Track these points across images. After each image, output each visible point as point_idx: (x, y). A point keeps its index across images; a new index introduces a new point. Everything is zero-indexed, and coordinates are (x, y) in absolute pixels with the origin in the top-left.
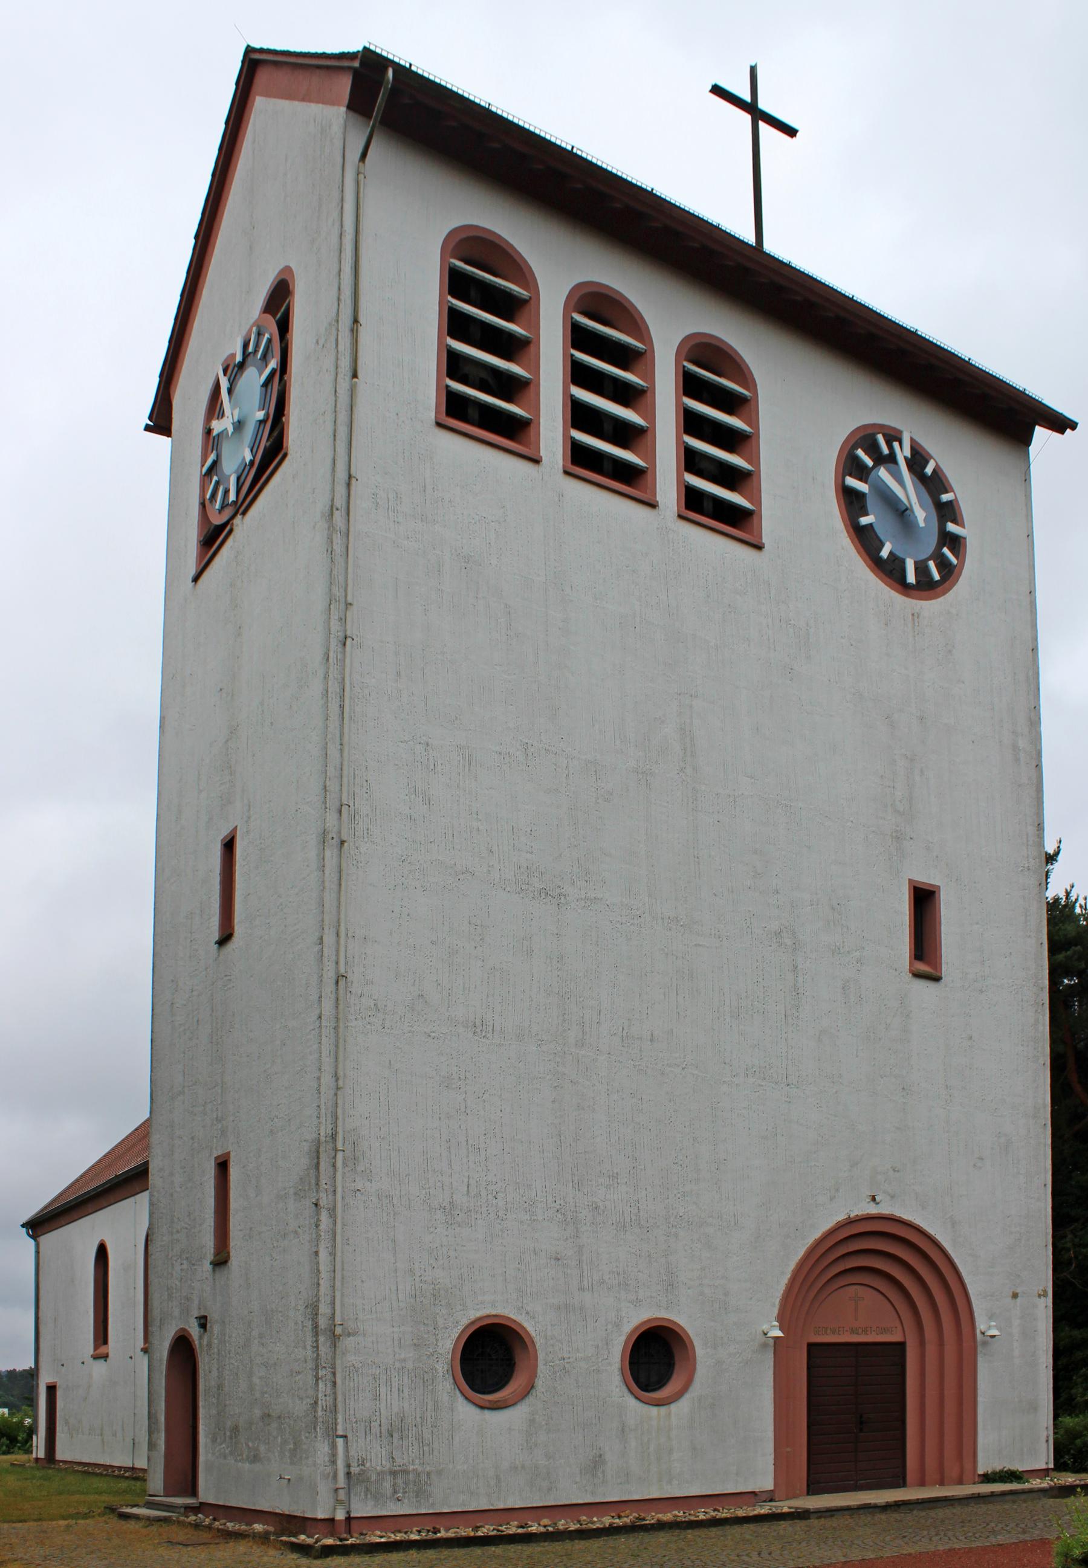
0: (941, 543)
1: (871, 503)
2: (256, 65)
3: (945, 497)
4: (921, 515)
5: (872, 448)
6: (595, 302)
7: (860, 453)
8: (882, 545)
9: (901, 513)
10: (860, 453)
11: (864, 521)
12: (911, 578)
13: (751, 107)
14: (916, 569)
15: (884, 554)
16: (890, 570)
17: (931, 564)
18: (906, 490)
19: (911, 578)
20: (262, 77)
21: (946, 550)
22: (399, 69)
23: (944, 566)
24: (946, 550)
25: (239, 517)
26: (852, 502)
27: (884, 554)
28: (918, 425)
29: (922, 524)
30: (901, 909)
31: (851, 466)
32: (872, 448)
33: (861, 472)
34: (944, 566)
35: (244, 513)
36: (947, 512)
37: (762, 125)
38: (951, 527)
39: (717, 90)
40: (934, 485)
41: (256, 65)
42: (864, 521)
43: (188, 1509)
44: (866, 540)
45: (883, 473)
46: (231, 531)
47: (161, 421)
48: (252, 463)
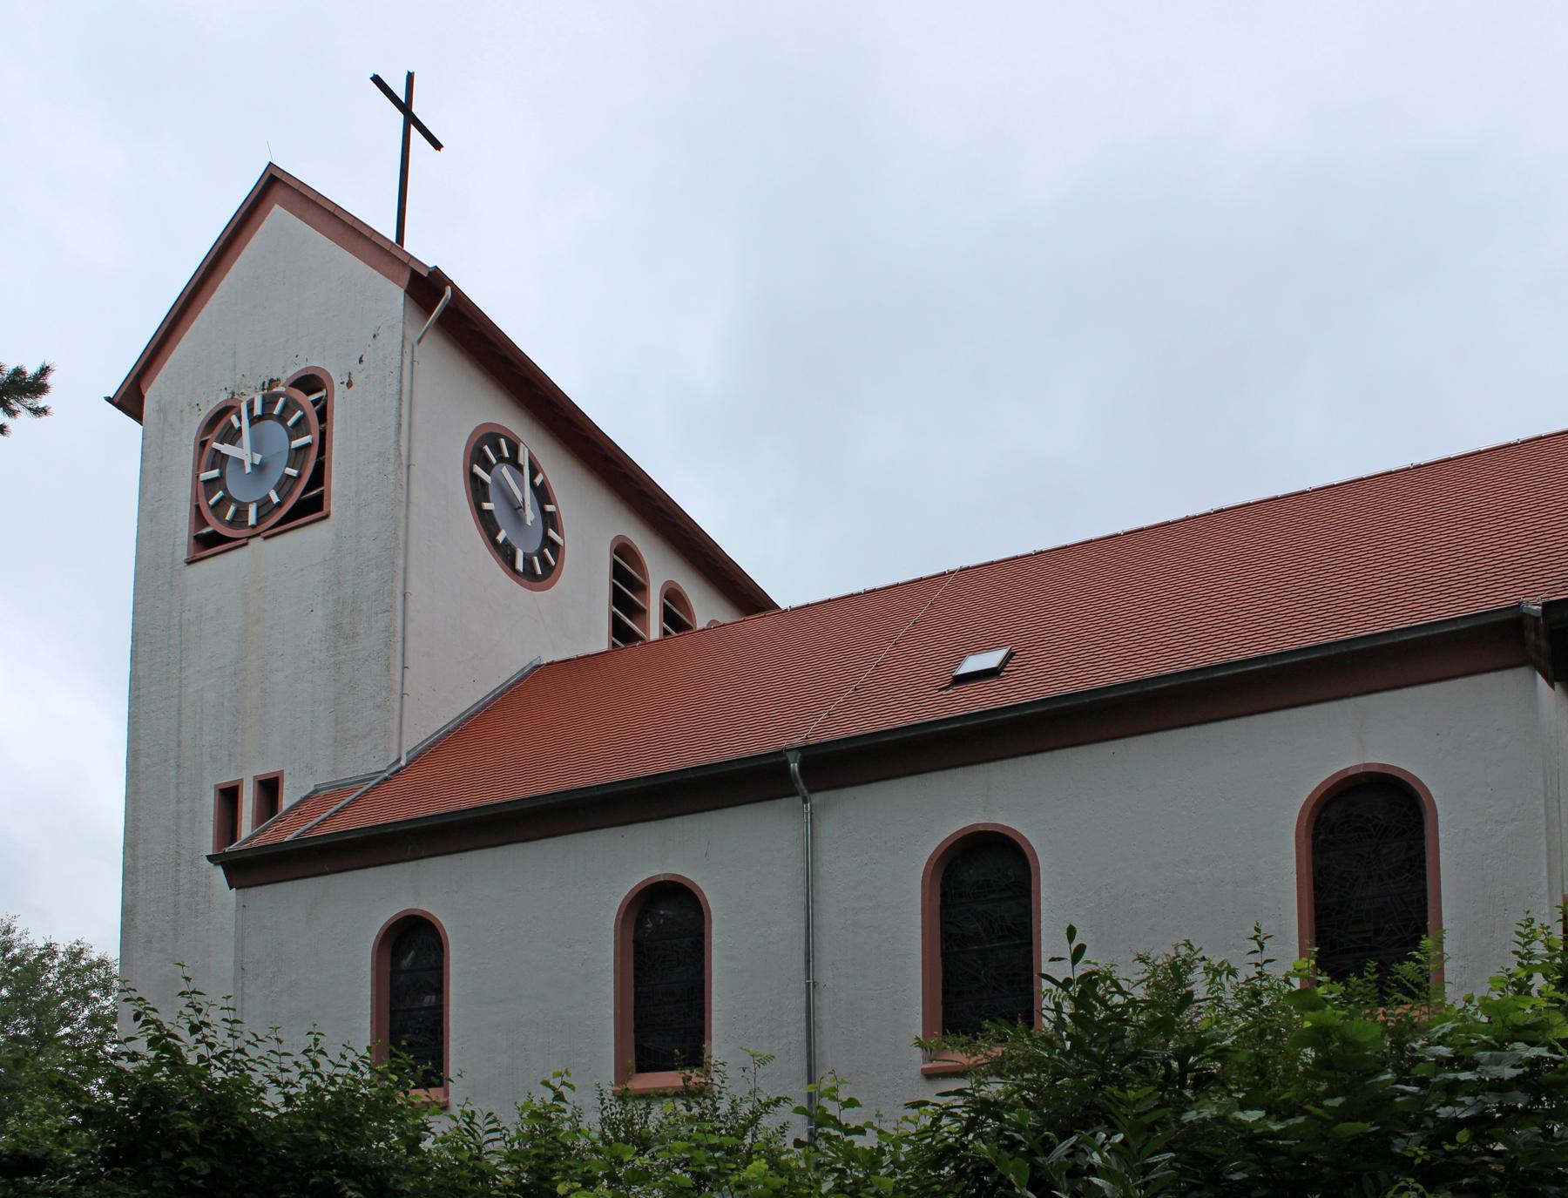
0: (543, 546)
1: (492, 492)
2: (273, 184)
3: (550, 508)
4: (531, 515)
5: (497, 449)
7: (486, 448)
9: (517, 510)
10: (486, 448)
11: (487, 506)
12: (520, 566)
13: (405, 107)
15: (500, 538)
16: (505, 553)
18: (526, 496)
19: (520, 566)
20: (278, 192)
22: (457, 292)
23: (544, 561)
25: (259, 539)
26: (478, 490)
27: (500, 538)
28: (533, 443)
30: (209, 804)
31: (476, 456)
32: (497, 449)
33: (488, 467)
34: (544, 561)
35: (266, 538)
36: (550, 520)
38: (552, 533)
39: (377, 80)
40: (542, 494)
41: (273, 184)
42: (487, 506)
44: (488, 524)
45: (505, 471)
47: (130, 400)
48: (279, 505)
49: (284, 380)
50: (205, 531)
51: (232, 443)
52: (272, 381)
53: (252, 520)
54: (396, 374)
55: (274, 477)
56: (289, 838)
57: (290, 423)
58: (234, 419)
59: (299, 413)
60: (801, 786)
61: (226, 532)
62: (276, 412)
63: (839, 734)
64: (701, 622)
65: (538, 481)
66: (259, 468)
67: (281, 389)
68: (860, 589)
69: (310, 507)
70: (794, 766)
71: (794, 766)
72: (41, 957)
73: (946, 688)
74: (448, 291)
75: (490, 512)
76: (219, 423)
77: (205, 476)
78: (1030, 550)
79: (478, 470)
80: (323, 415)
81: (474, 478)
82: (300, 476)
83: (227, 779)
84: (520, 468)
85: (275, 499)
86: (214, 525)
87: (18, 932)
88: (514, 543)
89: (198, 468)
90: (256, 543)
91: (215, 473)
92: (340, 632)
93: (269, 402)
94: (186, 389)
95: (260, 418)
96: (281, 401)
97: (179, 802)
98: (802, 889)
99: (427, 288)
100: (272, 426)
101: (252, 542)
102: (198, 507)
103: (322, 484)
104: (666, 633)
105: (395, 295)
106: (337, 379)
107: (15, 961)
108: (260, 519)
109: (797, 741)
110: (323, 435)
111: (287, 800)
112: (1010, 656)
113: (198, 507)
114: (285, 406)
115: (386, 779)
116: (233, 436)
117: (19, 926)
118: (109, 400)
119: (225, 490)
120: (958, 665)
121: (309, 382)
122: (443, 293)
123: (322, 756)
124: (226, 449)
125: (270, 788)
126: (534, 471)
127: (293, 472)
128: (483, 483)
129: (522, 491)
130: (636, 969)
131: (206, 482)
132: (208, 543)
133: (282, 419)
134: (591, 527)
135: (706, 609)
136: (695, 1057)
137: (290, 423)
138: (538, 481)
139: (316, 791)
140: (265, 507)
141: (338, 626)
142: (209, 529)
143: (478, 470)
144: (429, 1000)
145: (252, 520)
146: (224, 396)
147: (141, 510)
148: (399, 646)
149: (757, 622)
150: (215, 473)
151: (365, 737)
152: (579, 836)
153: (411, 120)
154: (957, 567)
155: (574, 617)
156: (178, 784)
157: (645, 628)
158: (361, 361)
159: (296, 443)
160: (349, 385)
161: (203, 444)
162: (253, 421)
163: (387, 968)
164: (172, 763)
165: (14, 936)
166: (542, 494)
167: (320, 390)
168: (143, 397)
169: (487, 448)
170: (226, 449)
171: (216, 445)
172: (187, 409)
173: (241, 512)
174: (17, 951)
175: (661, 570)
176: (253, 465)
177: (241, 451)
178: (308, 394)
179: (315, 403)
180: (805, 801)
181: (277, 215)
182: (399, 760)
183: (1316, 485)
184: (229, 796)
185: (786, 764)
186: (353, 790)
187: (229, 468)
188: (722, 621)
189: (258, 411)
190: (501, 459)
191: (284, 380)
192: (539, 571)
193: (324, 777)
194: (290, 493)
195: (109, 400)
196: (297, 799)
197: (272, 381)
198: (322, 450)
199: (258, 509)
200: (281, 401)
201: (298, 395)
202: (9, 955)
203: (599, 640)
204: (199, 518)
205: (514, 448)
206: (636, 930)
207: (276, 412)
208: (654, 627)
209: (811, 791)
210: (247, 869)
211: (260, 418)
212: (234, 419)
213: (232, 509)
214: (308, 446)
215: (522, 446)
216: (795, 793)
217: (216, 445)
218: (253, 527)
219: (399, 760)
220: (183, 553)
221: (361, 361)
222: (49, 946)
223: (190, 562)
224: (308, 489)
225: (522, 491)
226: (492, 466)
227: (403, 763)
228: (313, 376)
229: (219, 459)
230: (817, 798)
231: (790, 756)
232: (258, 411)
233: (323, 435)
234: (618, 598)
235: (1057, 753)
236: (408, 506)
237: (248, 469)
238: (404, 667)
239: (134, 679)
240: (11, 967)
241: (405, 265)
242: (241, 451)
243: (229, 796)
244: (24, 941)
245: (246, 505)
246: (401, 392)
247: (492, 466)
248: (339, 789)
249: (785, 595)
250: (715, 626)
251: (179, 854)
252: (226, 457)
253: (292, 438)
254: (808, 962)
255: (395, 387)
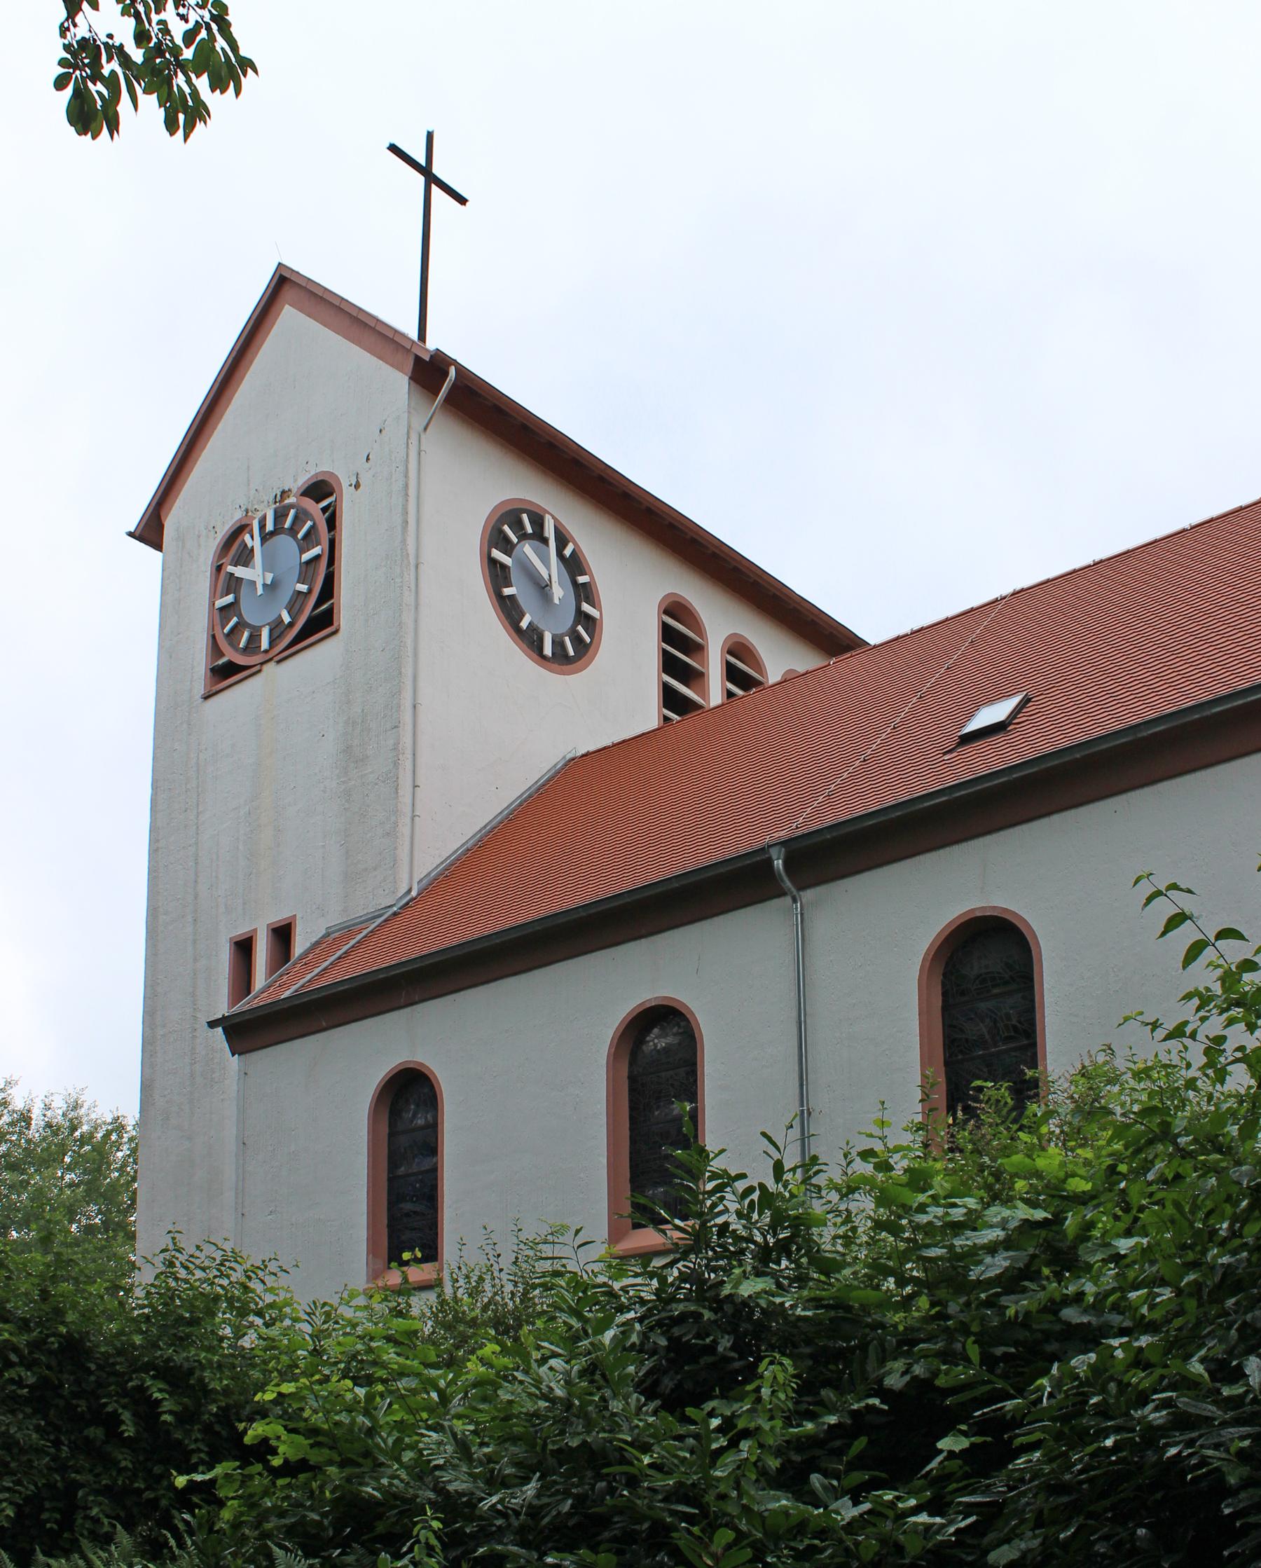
0: (577, 622)
1: (514, 576)
2: (284, 285)
3: (582, 579)
5: (518, 526)
6: (738, 648)
7: (506, 528)
8: (522, 615)
9: (543, 589)
10: (506, 528)
11: (507, 591)
12: (548, 650)
13: (426, 171)
14: (553, 642)
15: (524, 624)
16: (531, 640)
17: (567, 639)
18: (551, 570)
19: (548, 650)
20: (288, 293)
21: (580, 628)
22: (461, 370)
23: (577, 640)
24: (580, 628)
25: (272, 664)
26: (497, 575)
27: (524, 624)
28: (561, 509)
29: (557, 601)
30: (224, 958)
31: (496, 538)
32: (518, 526)
33: (508, 547)
34: (577, 640)
35: (279, 662)
36: (585, 593)
37: (423, 162)
38: (586, 607)
40: (574, 565)
41: (284, 285)
42: (507, 591)
43: (824, 1283)
44: (509, 610)
45: (528, 549)
46: (260, 671)
47: (150, 531)
48: (291, 625)
49: (294, 490)
50: (220, 662)
51: (246, 565)
52: (283, 492)
53: (265, 644)
54: (402, 468)
55: (285, 596)
56: (287, 994)
57: (300, 536)
58: (247, 538)
59: (309, 523)
60: (788, 883)
61: (240, 660)
62: (287, 525)
63: (828, 821)
64: (773, 675)
65: (568, 552)
66: (271, 588)
67: (292, 500)
68: (907, 630)
69: (320, 623)
70: (779, 864)
71: (779, 864)
72: (108, 1134)
73: (950, 752)
74: (452, 371)
75: (512, 597)
76: (233, 546)
77: (221, 602)
78: (1089, 561)
79: (496, 554)
80: (332, 523)
81: (493, 562)
82: (310, 591)
83: (241, 931)
84: (545, 541)
85: (287, 619)
86: (230, 655)
87: (86, 1106)
88: (541, 626)
89: (214, 596)
90: (270, 668)
91: (230, 598)
92: (351, 756)
93: (280, 516)
94: (201, 517)
95: (272, 534)
96: (292, 512)
97: (195, 960)
98: (794, 1003)
99: (430, 372)
100: (284, 541)
101: (265, 668)
102: (214, 637)
103: (331, 597)
104: (730, 694)
105: (399, 382)
106: (345, 481)
107: (83, 1140)
108: (272, 642)
109: (782, 834)
110: (332, 543)
111: (300, 945)
112: (1026, 701)
113: (214, 637)
114: (296, 518)
115: (395, 914)
116: (245, 557)
117: (87, 1099)
118: (130, 534)
119: (240, 616)
120: (970, 716)
121: (320, 489)
122: (446, 374)
123: (329, 899)
124: (239, 571)
125: (283, 934)
126: (562, 540)
127: (303, 588)
128: (504, 567)
129: (547, 564)
130: (631, 1108)
131: (222, 609)
132: (225, 673)
133: (293, 531)
134: (635, 594)
135: (779, 658)
136: (431, 1253)
137: (300, 536)
138: (568, 552)
139: (328, 934)
140: (278, 629)
141: (348, 750)
142: (224, 660)
143: (496, 554)
144: (427, 1164)
145: (265, 644)
146: (238, 515)
147: (161, 647)
148: (408, 765)
149: (693, 719)
150: (230, 598)
151: (375, 869)
152: (956, 850)
153: (431, 179)
154: (1010, 590)
155: (618, 695)
156: (195, 941)
157: (704, 693)
158: (368, 459)
159: (306, 556)
160: (357, 486)
161: (219, 568)
162: (265, 537)
163: (384, 1130)
164: (190, 918)
165: (82, 1111)
166: (574, 565)
167: (331, 494)
168: (162, 527)
169: (509, 527)
170: (239, 571)
171: (230, 569)
172: (204, 532)
173: (255, 638)
174: (85, 1128)
175: (720, 621)
176: (265, 585)
177: (254, 573)
178: (318, 502)
179: (324, 510)
180: (795, 900)
181: (289, 317)
182: (410, 890)
183: (1195, 521)
184: (244, 947)
185: (769, 861)
186: (360, 931)
187: (244, 591)
188: (801, 670)
189: (270, 527)
190: (523, 537)
191: (294, 490)
192: (572, 650)
193: (334, 919)
194: (301, 611)
195: (130, 534)
196: (308, 945)
197: (283, 492)
198: (331, 561)
199: (271, 631)
200: (292, 512)
201: (308, 504)
202: (77, 1134)
203: (646, 715)
204: (216, 650)
205: (538, 522)
206: (631, 1065)
207: (287, 525)
208: (715, 689)
209: (802, 887)
210: (248, 1031)
211: (272, 534)
212: (247, 538)
213: (246, 634)
214: (318, 557)
215: (547, 517)
216: (782, 893)
217: (230, 569)
218: (266, 652)
219: (410, 890)
220: (200, 688)
221: (368, 459)
222: (116, 1119)
223: (207, 697)
224: (319, 603)
225: (547, 564)
226: (513, 546)
227: (414, 893)
228: (323, 482)
229: (233, 583)
230: (808, 895)
231: (774, 852)
232: (270, 527)
233: (332, 543)
234: (670, 665)
235: (536, 972)
236: (416, 608)
237: (260, 591)
238: (415, 786)
239: (153, 829)
240: (81, 1147)
241: (409, 351)
242: (254, 573)
243: (244, 947)
244: (93, 1116)
245: (259, 629)
246: (406, 486)
247: (513, 546)
248: (348, 930)
249: (873, 627)
250: (790, 679)
251: (195, 1018)
252: (239, 580)
253: (302, 551)
254: (801, 1085)
255: (401, 483)
